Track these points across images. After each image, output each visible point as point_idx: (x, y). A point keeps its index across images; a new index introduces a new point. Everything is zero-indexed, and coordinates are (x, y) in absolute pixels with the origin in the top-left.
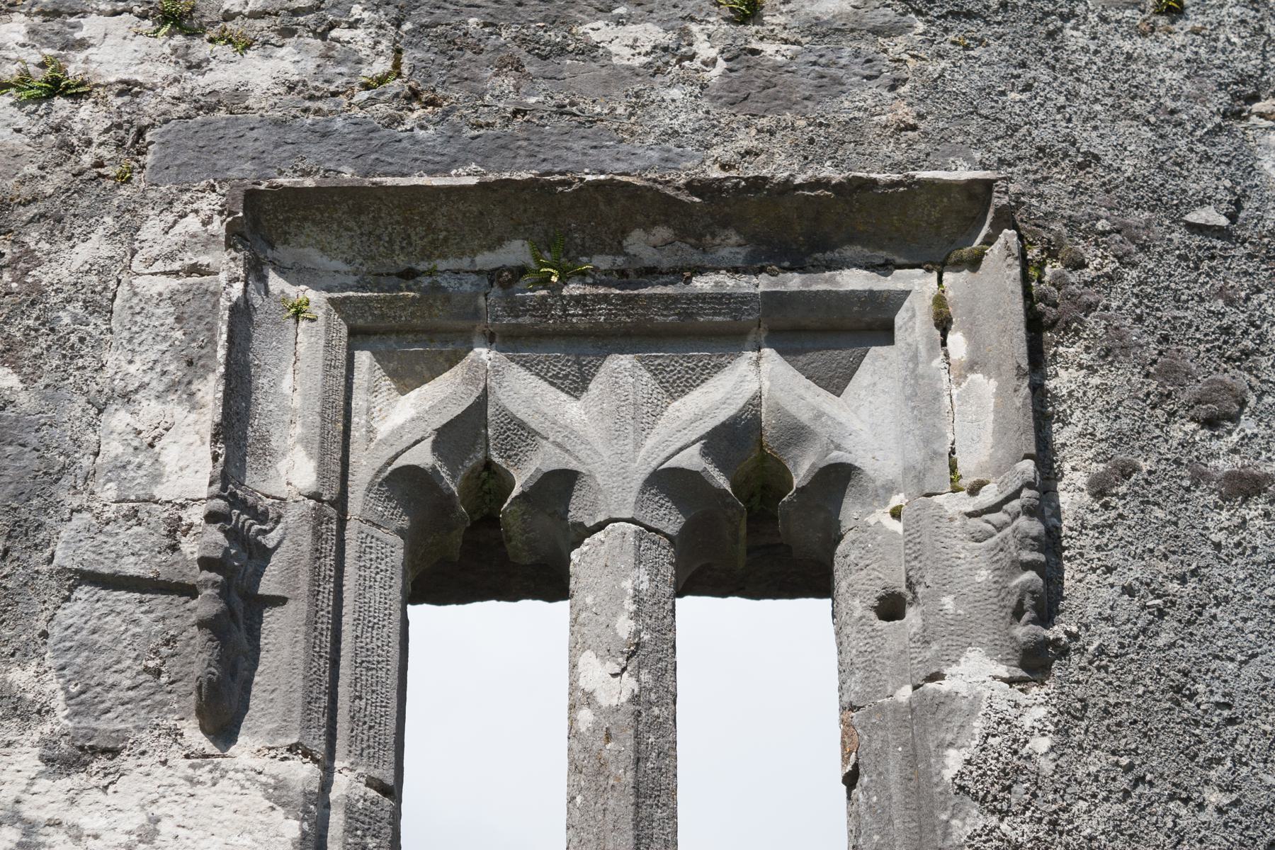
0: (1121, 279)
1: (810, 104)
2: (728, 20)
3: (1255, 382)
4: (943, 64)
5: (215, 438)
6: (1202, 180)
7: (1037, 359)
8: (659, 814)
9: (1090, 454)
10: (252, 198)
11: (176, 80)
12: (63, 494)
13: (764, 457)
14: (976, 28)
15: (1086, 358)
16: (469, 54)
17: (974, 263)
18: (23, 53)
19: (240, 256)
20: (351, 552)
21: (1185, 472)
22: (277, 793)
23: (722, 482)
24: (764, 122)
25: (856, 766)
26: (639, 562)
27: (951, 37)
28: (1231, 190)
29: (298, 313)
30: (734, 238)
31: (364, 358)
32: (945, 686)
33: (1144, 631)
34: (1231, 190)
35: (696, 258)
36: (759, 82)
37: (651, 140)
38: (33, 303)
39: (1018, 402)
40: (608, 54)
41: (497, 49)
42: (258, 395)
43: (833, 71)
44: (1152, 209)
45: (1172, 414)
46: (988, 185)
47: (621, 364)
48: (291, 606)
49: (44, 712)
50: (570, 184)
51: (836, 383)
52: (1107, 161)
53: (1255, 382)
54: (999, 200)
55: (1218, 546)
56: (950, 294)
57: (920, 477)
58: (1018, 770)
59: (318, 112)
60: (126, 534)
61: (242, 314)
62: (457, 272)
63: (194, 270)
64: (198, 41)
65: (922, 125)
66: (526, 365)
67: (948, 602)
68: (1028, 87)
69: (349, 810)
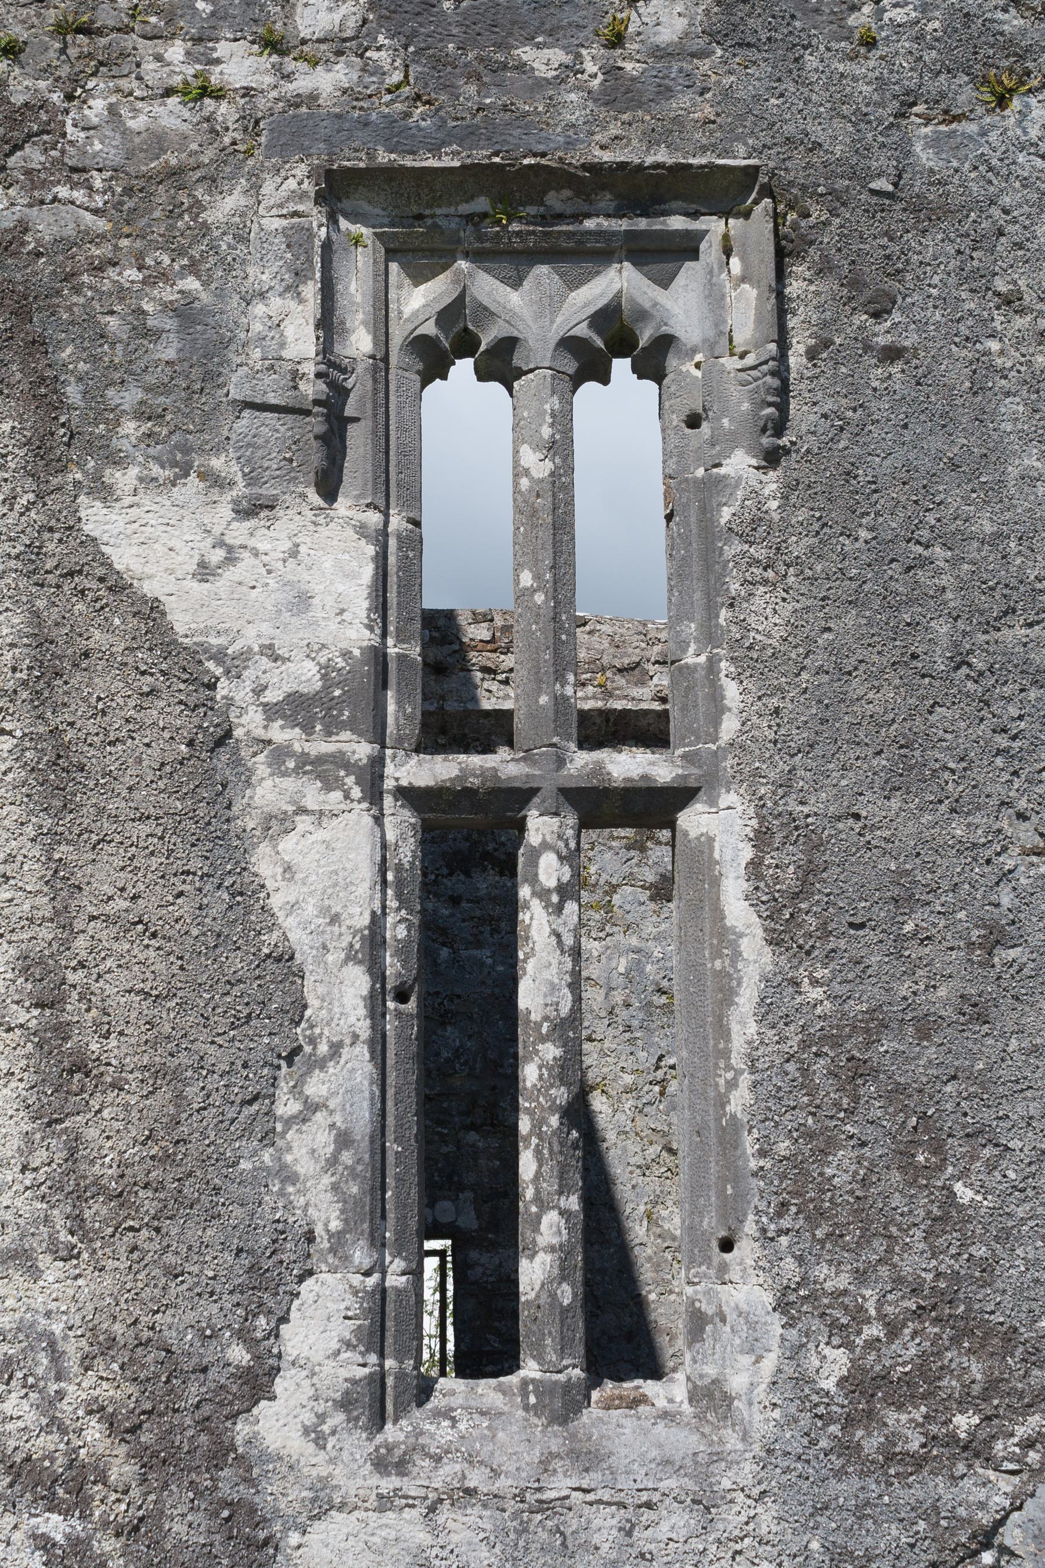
0: (830, 224)
1: (652, 104)
2: (605, 46)
3: (902, 289)
4: (733, 78)
5: (317, 327)
6: (880, 161)
7: (781, 274)
8: (566, 538)
9: (807, 333)
10: (329, 175)
11: (276, 87)
12: (231, 355)
13: (623, 325)
14: (752, 54)
15: (808, 274)
16: (449, 69)
17: (747, 215)
18: (184, 68)
19: (324, 210)
20: (392, 387)
21: (860, 345)
22: (362, 530)
23: (599, 343)
24: (625, 117)
25: (672, 511)
26: (553, 393)
27: (737, 60)
28: (896, 168)
29: (357, 241)
30: (608, 196)
31: (394, 267)
32: (722, 471)
33: (832, 440)
34: (896, 168)
35: (586, 208)
36: (622, 89)
37: (559, 130)
38: (204, 236)
39: (769, 307)
40: (533, 69)
41: (466, 65)
42: (338, 296)
43: (667, 81)
44: (850, 179)
45: (854, 309)
46: (756, 169)
47: (542, 270)
48: (362, 423)
49: (232, 484)
50: (513, 165)
51: (665, 282)
52: (826, 147)
53: (902, 289)
54: (763, 179)
55: (875, 390)
56: (732, 233)
57: (712, 346)
58: (761, 519)
59: (361, 109)
60: (269, 379)
61: (327, 246)
62: (447, 216)
63: (295, 214)
64: (286, 59)
65: (719, 120)
66: (487, 271)
67: (726, 422)
68: (782, 95)
69: (399, 537)
